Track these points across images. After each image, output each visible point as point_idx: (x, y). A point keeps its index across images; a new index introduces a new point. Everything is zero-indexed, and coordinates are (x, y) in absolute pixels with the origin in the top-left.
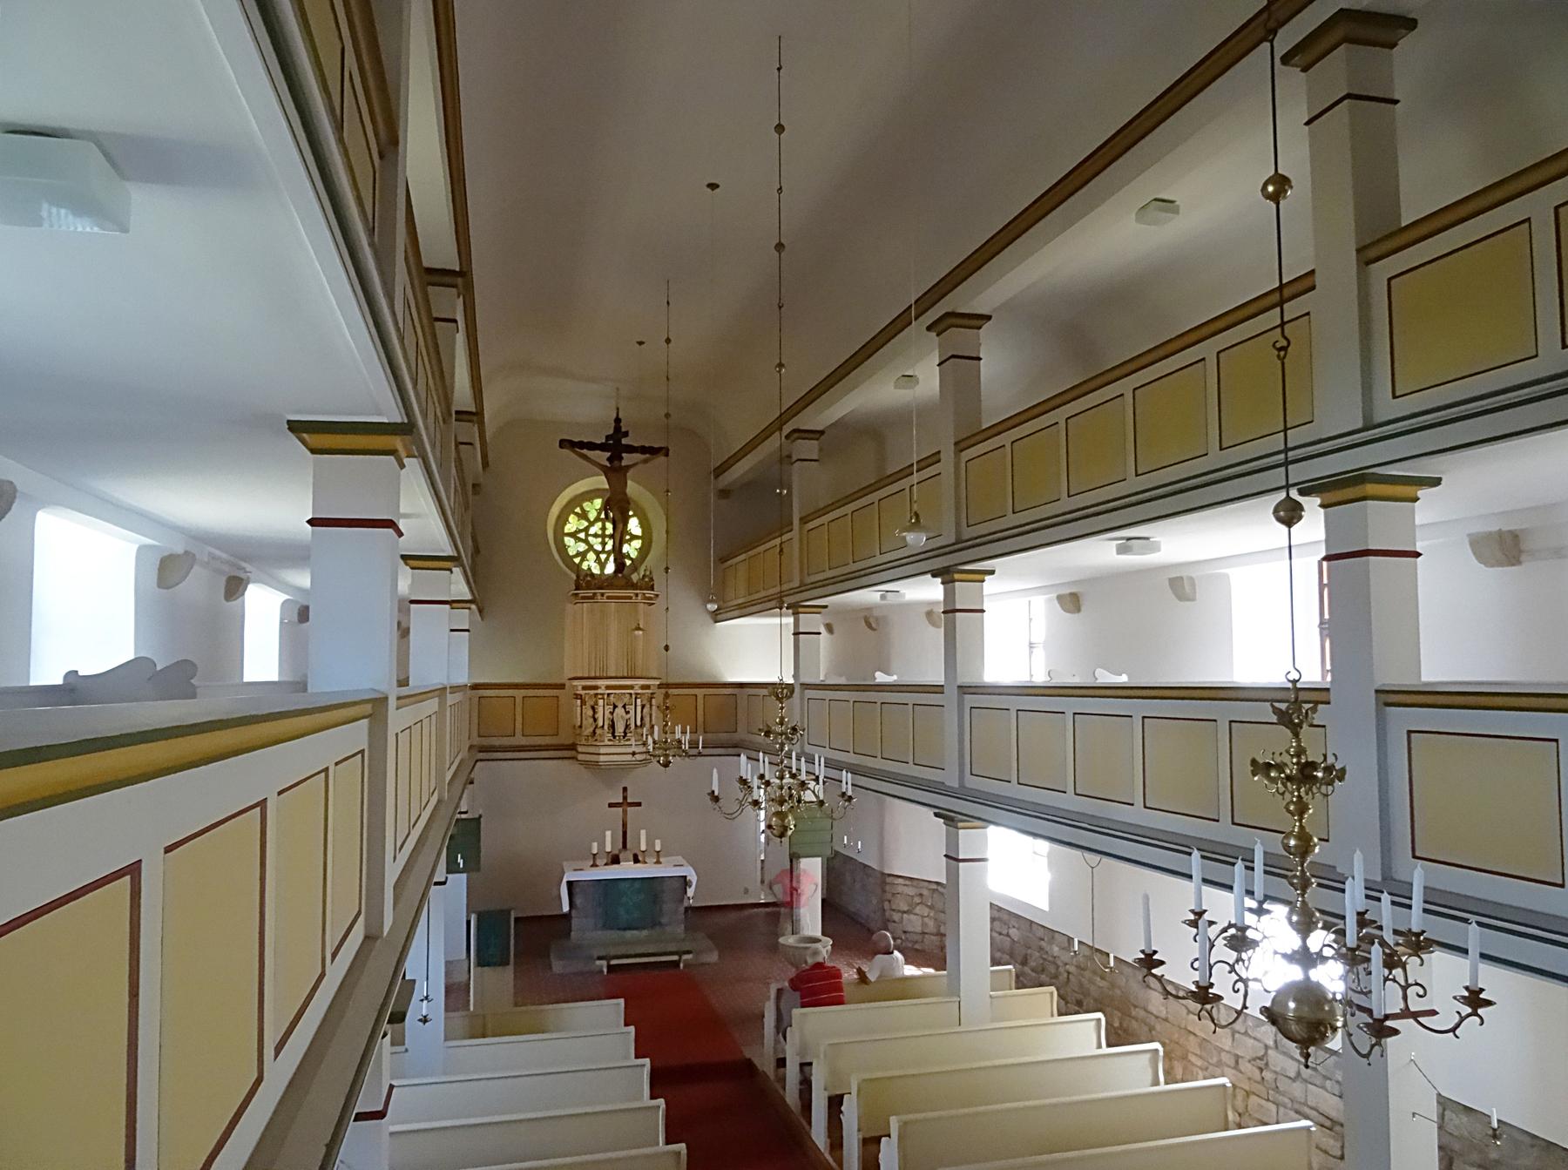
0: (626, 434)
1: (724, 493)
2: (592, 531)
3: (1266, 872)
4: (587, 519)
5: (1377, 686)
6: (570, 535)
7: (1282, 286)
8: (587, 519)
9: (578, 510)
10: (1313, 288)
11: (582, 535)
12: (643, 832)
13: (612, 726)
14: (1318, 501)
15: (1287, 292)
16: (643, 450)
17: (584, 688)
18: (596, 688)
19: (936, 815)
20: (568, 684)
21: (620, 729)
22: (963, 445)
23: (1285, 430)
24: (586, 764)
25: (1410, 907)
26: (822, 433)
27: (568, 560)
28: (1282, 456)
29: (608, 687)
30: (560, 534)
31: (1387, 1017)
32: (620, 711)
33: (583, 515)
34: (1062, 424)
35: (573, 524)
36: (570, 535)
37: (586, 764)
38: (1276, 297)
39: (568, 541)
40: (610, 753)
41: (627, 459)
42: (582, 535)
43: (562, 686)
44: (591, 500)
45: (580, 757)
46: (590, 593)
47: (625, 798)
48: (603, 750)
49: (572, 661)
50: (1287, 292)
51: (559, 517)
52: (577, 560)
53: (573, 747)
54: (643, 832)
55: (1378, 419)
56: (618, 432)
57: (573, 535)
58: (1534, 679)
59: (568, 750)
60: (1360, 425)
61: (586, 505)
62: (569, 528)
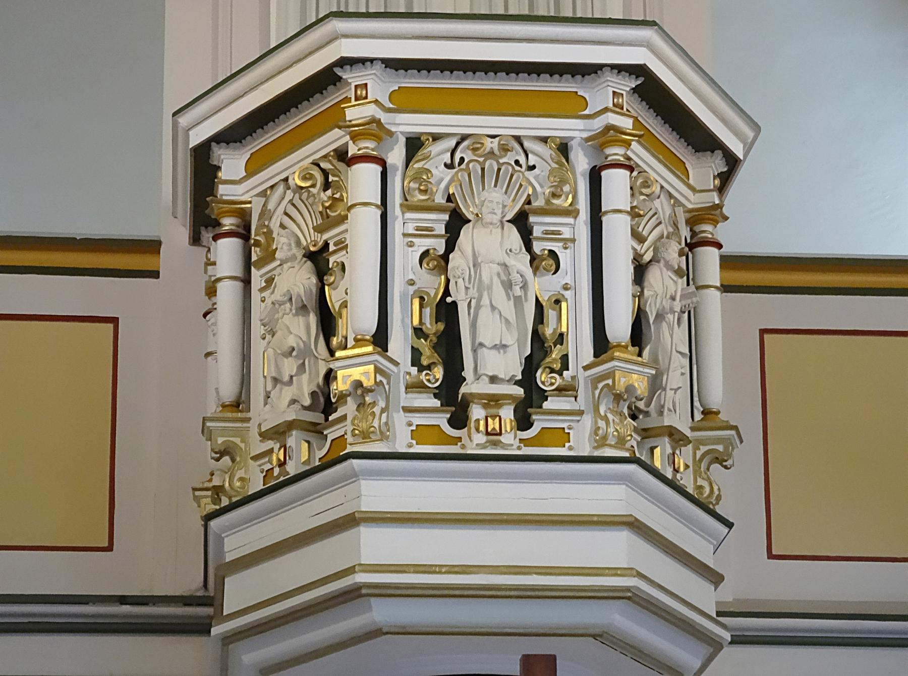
13: (445, 336)
21: (494, 358)
32: (489, 243)
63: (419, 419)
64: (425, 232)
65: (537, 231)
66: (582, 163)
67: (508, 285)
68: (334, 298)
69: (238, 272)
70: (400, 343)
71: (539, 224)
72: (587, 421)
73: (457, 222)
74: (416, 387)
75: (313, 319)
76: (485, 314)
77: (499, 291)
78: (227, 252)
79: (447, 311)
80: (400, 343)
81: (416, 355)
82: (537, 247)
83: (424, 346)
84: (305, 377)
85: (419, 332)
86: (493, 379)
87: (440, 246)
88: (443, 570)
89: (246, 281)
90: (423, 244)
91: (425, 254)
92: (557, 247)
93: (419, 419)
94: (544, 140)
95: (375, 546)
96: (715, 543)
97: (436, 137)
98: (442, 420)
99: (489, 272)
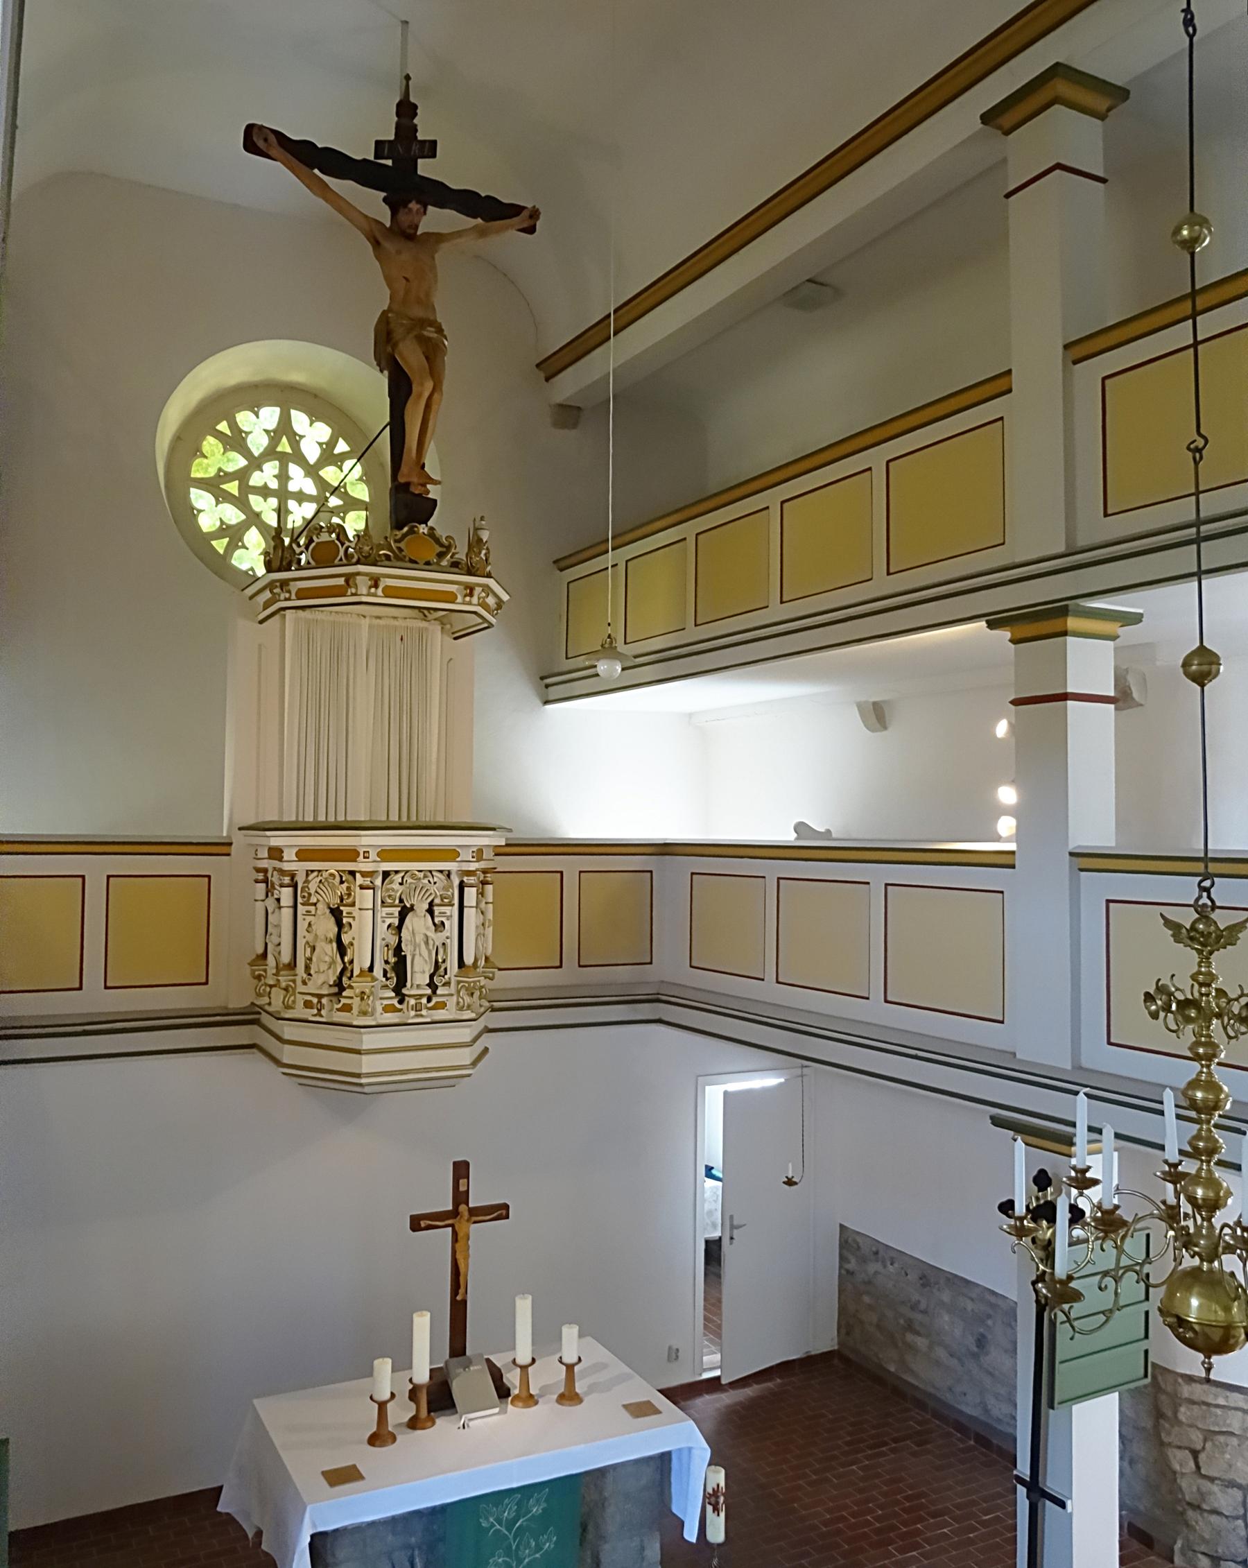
0: (430, 149)
1: (568, 415)
2: (256, 479)
3: (1178, 1117)
4: (246, 452)
5: (1072, 846)
6: (204, 484)
7: (1194, 293)
8: (246, 452)
9: (223, 427)
10: (1010, 391)
11: (233, 487)
12: (524, 1307)
13: (400, 967)
14: (1008, 635)
15: (1187, 307)
16: (469, 202)
17: (304, 854)
18: (351, 854)
19: (997, 1122)
20: (239, 839)
21: (419, 973)
22: (563, 564)
23: (1197, 493)
24: (297, 1071)
25: (1162, 1113)
26: (1120, 94)
27: (199, 542)
28: (1194, 530)
29: (386, 854)
30: (179, 483)
31: (1027, 1207)
32: (418, 924)
33: (236, 441)
34: (622, 567)
35: (215, 457)
36: (204, 484)
37: (297, 1071)
38: (1201, 302)
39: (200, 499)
40: (389, 1046)
41: (436, 219)
42: (284, 446)
43: (221, 848)
44: (254, 408)
45: (289, 1054)
46: (331, 576)
47: (460, 1197)
48: (370, 1040)
49: (244, 784)
50: (1187, 307)
51: (178, 439)
52: (220, 545)
53: (250, 1017)
54: (524, 1307)
55: (1082, 542)
56: (406, 145)
57: (213, 485)
58: (91, 833)
59: (242, 1025)
60: (1061, 549)
61: (244, 419)
62: (202, 469)
63: (386, 1002)
64: (390, 915)
65: (436, 913)
66: (456, 882)
67: (427, 943)
68: (346, 939)
69: (291, 904)
70: (378, 972)
71: (437, 910)
72: (455, 998)
73: (404, 912)
74: (386, 986)
75: (335, 945)
76: (417, 958)
77: (423, 946)
78: (286, 894)
79: (398, 950)
80: (378, 972)
81: (385, 973)
82: (437, 920)
83: (388, 967)
84: (331, 971)
85: (387, 962)
86: (418, 986)
87: (396, 922)
88: (423, 1224)
89: (295, 907)
90: (388, 921)
91: (389, 926)
92: (444, 919)
93: (386, 1002)
94: (441, 871)
95: (367, 1064)
96: (404, 819)
97: (397, 872)
98: (395, 1002)
99: (419, 939)
